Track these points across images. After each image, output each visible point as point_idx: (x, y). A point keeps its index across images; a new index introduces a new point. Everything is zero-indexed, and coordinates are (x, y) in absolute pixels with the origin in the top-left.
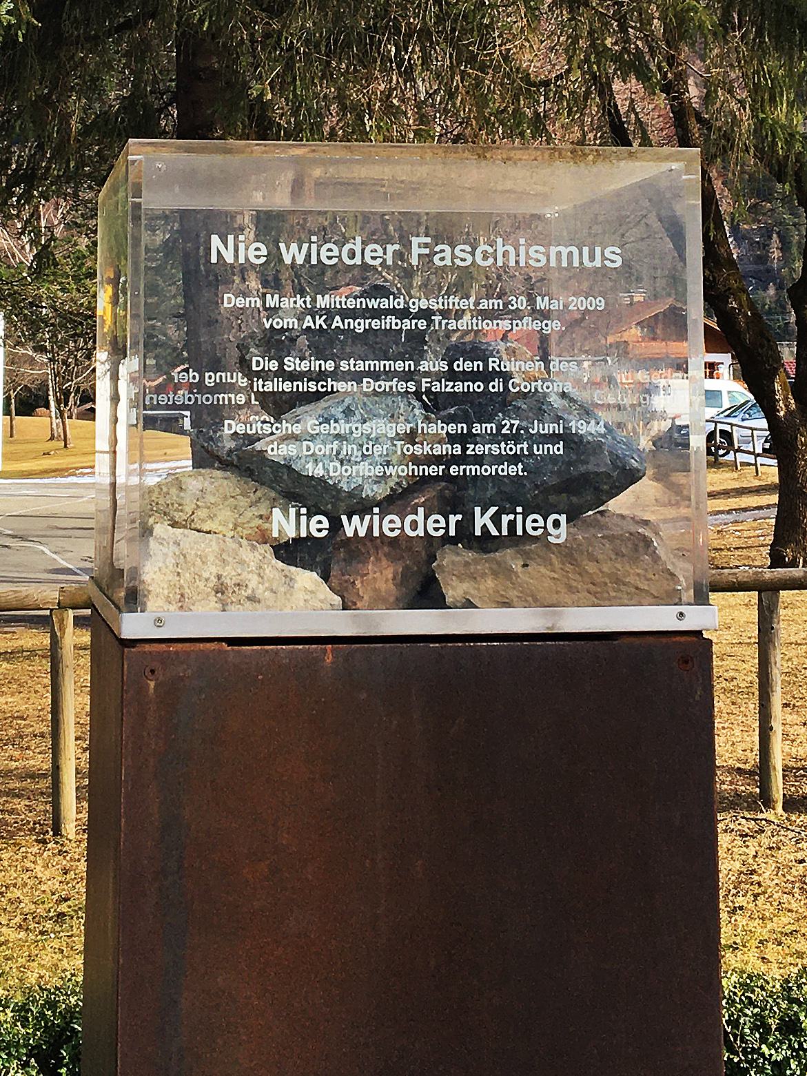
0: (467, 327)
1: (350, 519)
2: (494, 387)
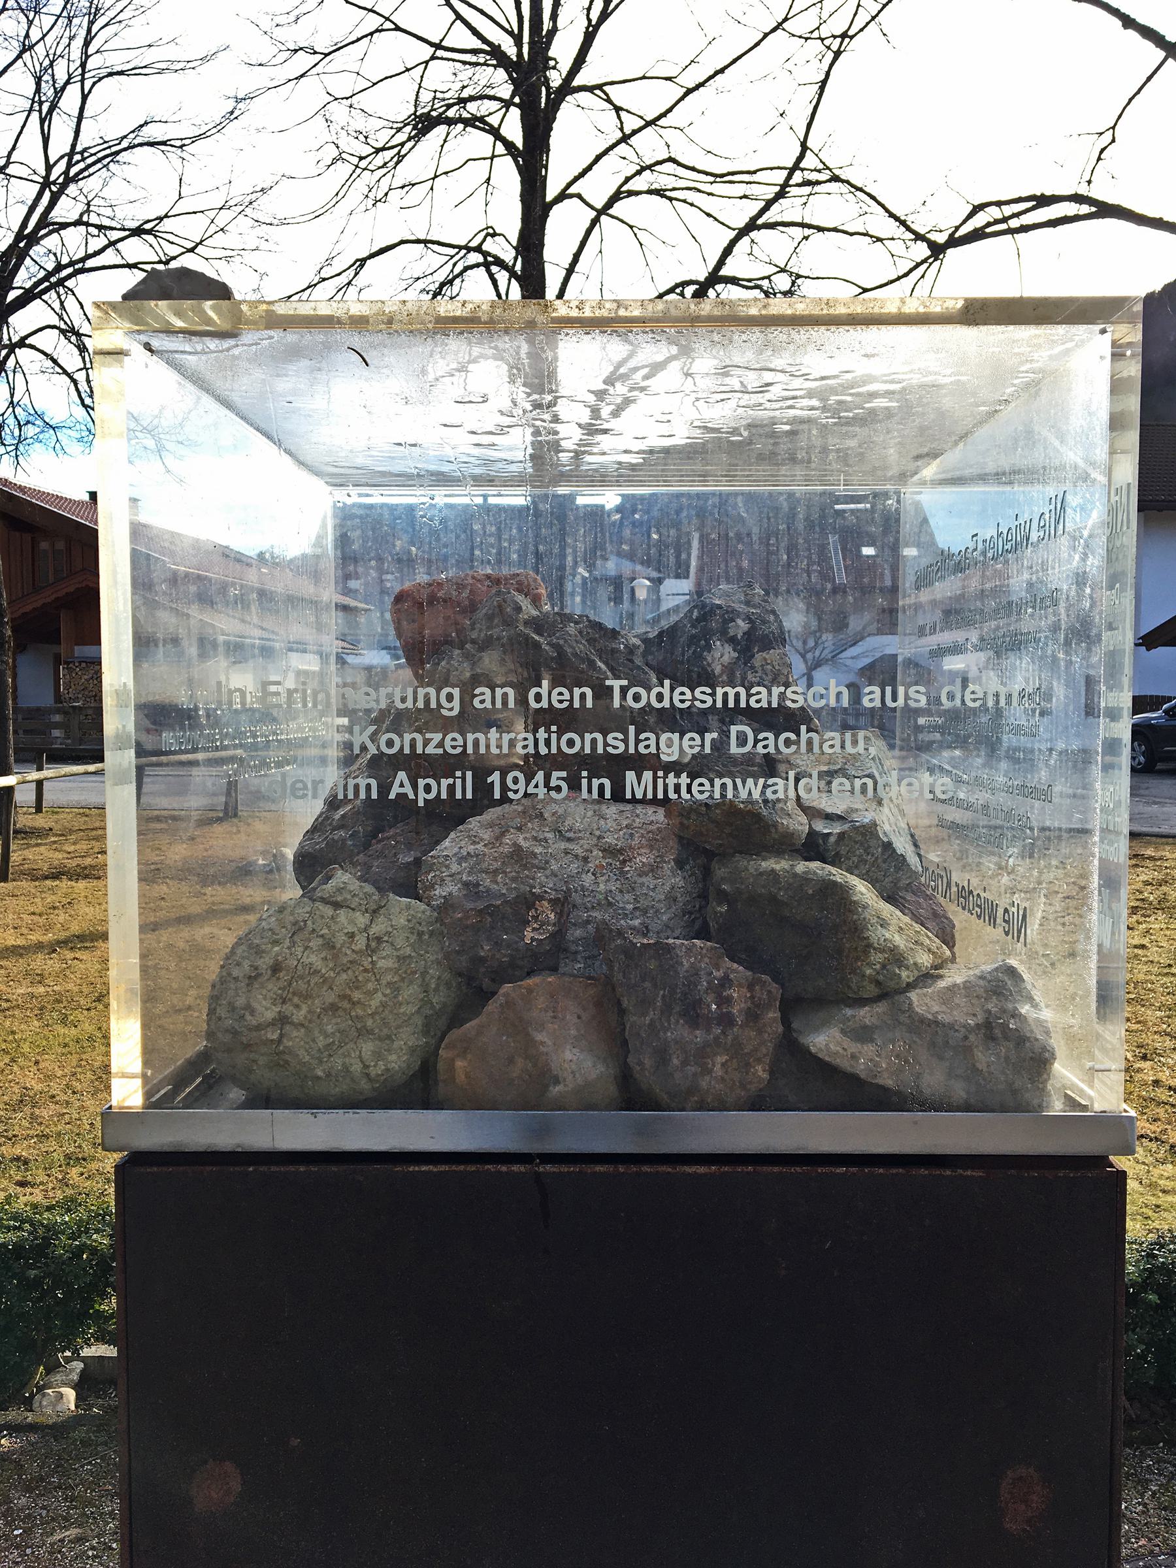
2: (538, 697)
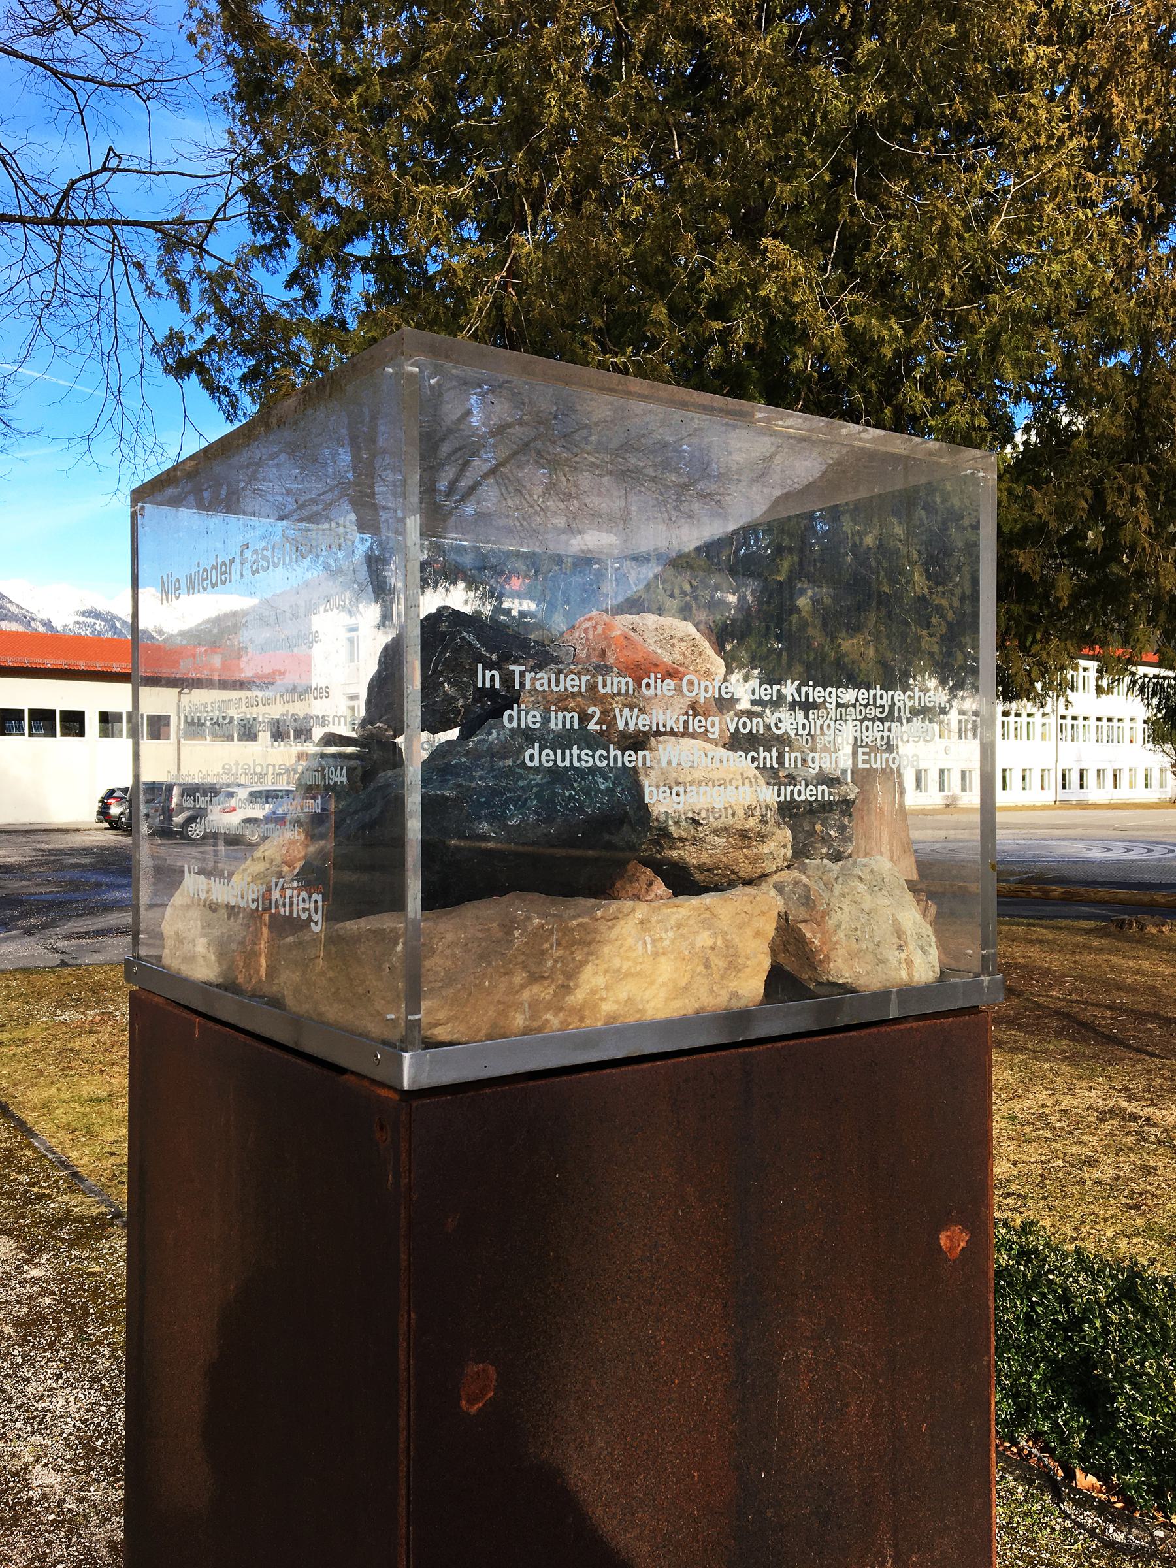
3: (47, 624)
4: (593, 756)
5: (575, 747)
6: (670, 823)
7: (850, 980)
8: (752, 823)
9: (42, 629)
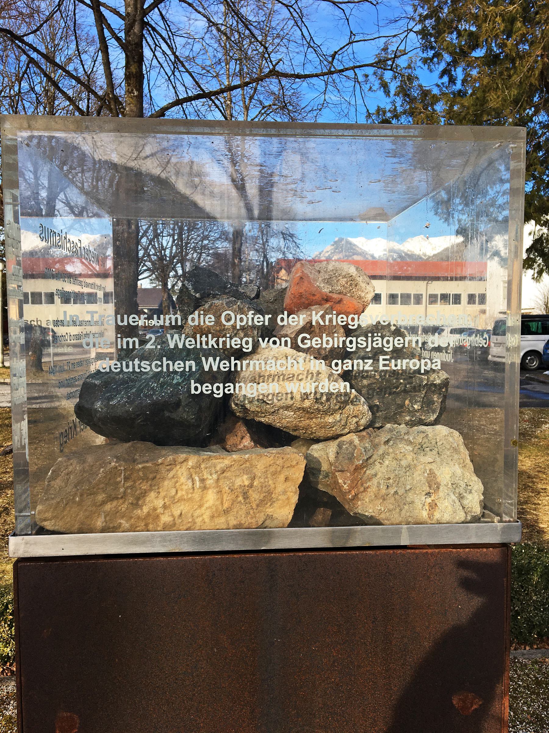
0: (164, 322)
1: (207, 360)
2: (193, 320)
3: (372, 256)
4: (150, 365)
5: (136, 360)
6: (246, 402)
7: (373, 514)
8: (307, 404)
9: (370, 258)
